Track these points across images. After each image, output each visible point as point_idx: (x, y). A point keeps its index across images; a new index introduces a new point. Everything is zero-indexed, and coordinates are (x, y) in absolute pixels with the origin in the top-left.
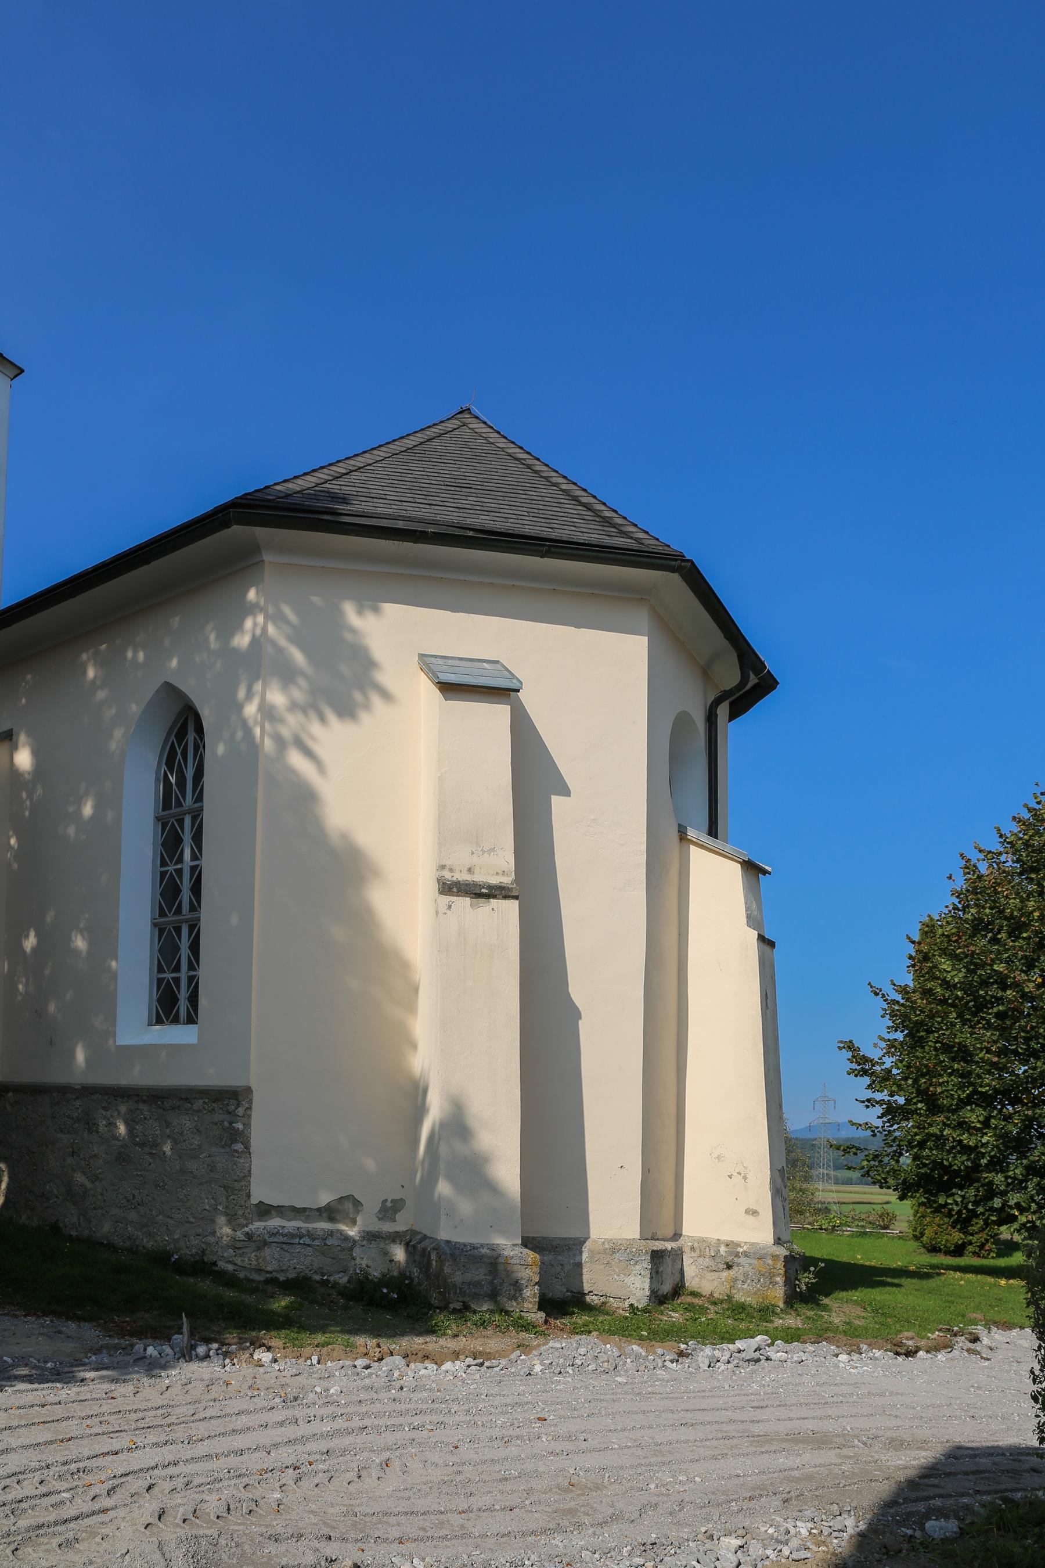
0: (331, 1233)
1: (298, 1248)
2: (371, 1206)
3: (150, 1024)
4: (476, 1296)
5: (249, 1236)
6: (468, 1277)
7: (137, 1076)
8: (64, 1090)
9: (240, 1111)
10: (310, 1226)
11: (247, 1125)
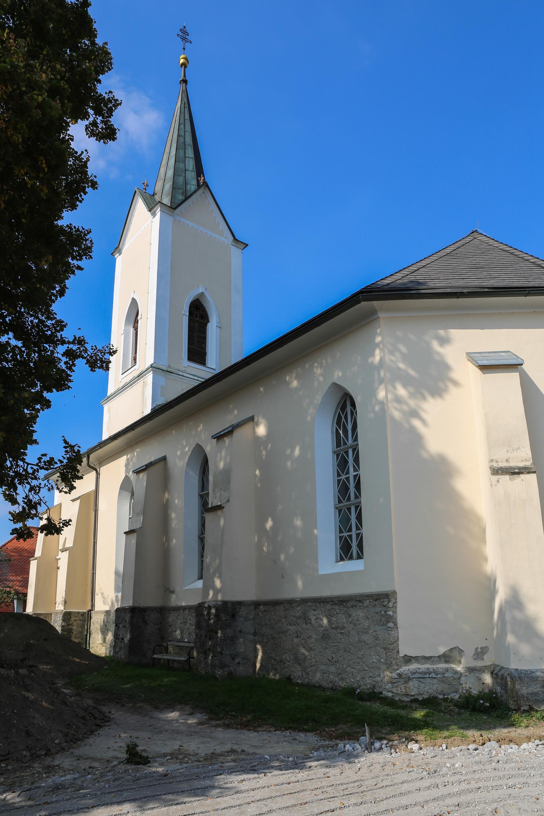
0: (447, 670)
1: (429, 680)
2: (469, 651)
3: (337, 562)
5: (400, 675)
6: (530, 690)
7: (326, 592)
8: (291, 602)
9: (391, 605)
10: (435, 667)
11: (395, 612)
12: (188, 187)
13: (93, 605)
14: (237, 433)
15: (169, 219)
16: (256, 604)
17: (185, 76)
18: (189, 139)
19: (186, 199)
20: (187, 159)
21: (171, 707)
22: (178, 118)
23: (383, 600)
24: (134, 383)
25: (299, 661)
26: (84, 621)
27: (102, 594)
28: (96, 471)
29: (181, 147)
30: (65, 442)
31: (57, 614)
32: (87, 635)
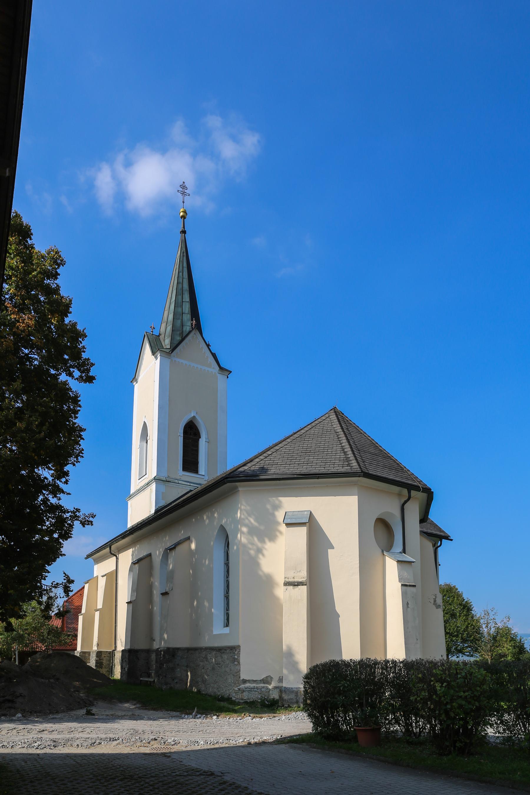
0: (264, 687)
1: (253, 692)
2: (276, 678)
3: (224, 627)
4: (293, 703)
5: (239, 689)
6: (289, 697)
7: (216, 644)
8: (201, 649)
9: (236, 653)
10: (258, 685)
11: (239, 656)
12: (184, 329)
13: (116, 647)
14: (179, 549)
15: (167, 361)
16: (188, 650)
17: (184, 227)
18: (186, 286)
19: (183, 340)
20: (184, 303)
21: (127, 701)
22: (178, 267)
23: (234, 650)
24: (145, 488)
25: (204, 681)
26: (110, 657)
27: (121, 640)
28: (116, 556)
29: (179, 293)
30: (64, 573)
31: (93, 652)
32: (112, 666)
